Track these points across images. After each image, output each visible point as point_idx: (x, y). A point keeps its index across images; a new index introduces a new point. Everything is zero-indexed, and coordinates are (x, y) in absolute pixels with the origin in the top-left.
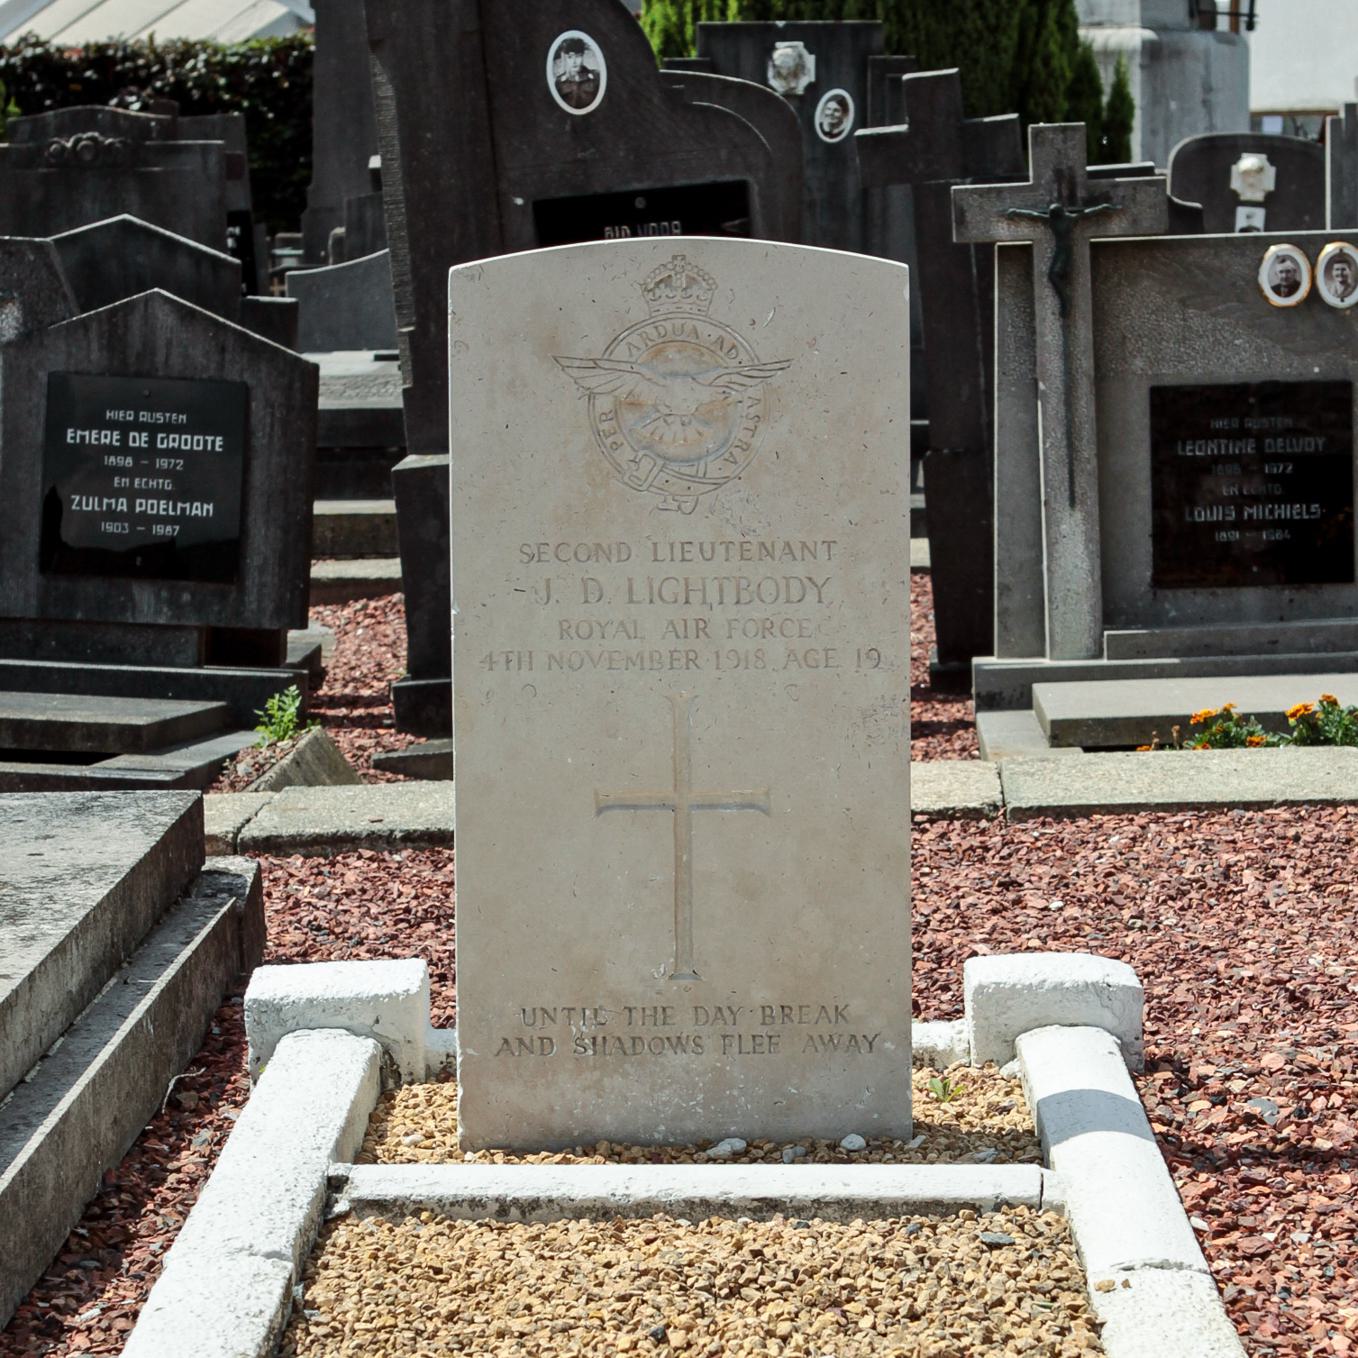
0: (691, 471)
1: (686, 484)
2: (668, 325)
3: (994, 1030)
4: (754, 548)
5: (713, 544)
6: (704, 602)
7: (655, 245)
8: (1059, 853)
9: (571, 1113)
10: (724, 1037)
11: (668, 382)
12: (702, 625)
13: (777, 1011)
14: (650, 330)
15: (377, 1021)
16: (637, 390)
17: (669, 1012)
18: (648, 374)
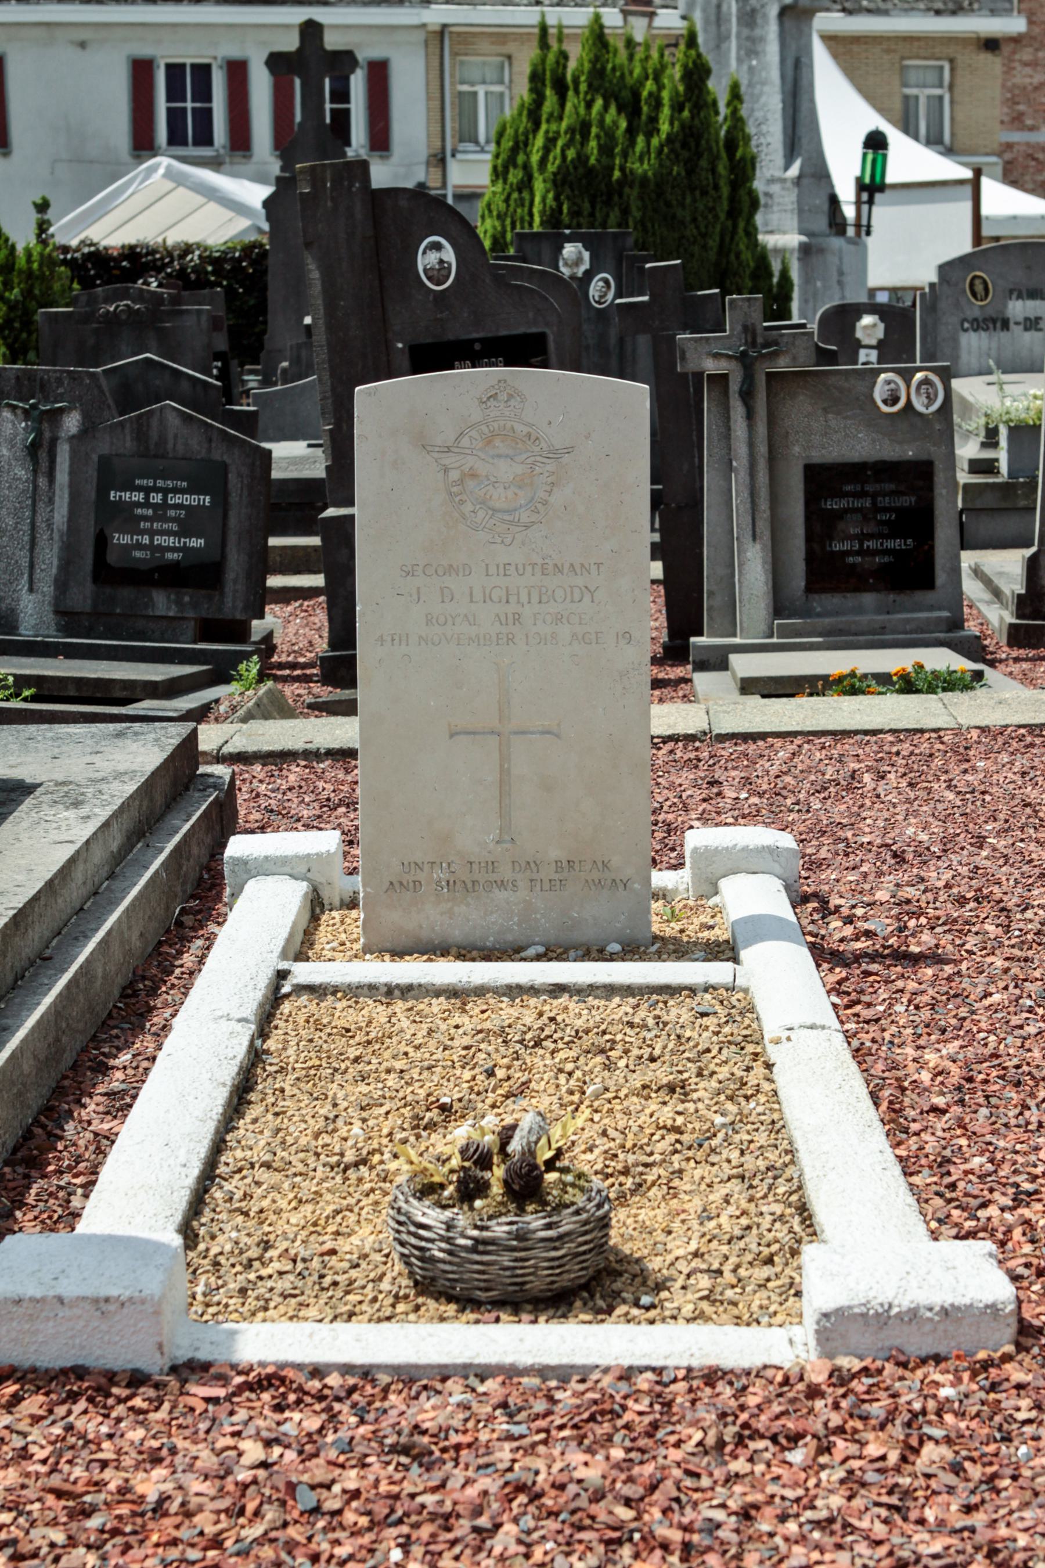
4: (550, 567)
7: (487, 373)
13: (565, 864)
14: (484, 428)
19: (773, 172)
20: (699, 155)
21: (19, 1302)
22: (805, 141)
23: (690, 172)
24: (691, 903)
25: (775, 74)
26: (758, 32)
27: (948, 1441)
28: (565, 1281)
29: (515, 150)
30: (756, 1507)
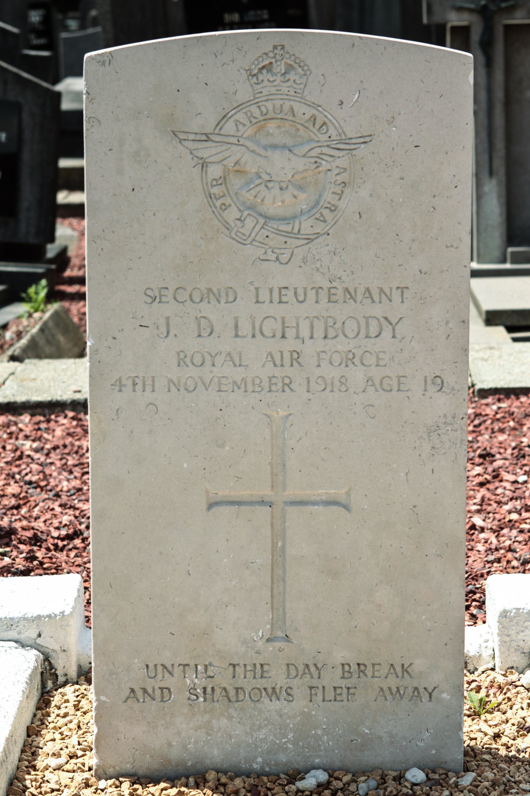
0: (289, 228)
1: (284, 239)
2: (269, 105)
3: (514, 644)
4: (340, 292)
5: (305, 289)
6: (297, 337)
7: (259, 37)
8: (512, 424)
9: (185, 747)
10: (311, 688)
11: (269, 153)
12: (295, 355)
13: (354, 667)
14: (254, 109)
15: (39, 635)
16: (243, 161)
17: (266, 668)
18: (252, 146)
24: (501, 680)
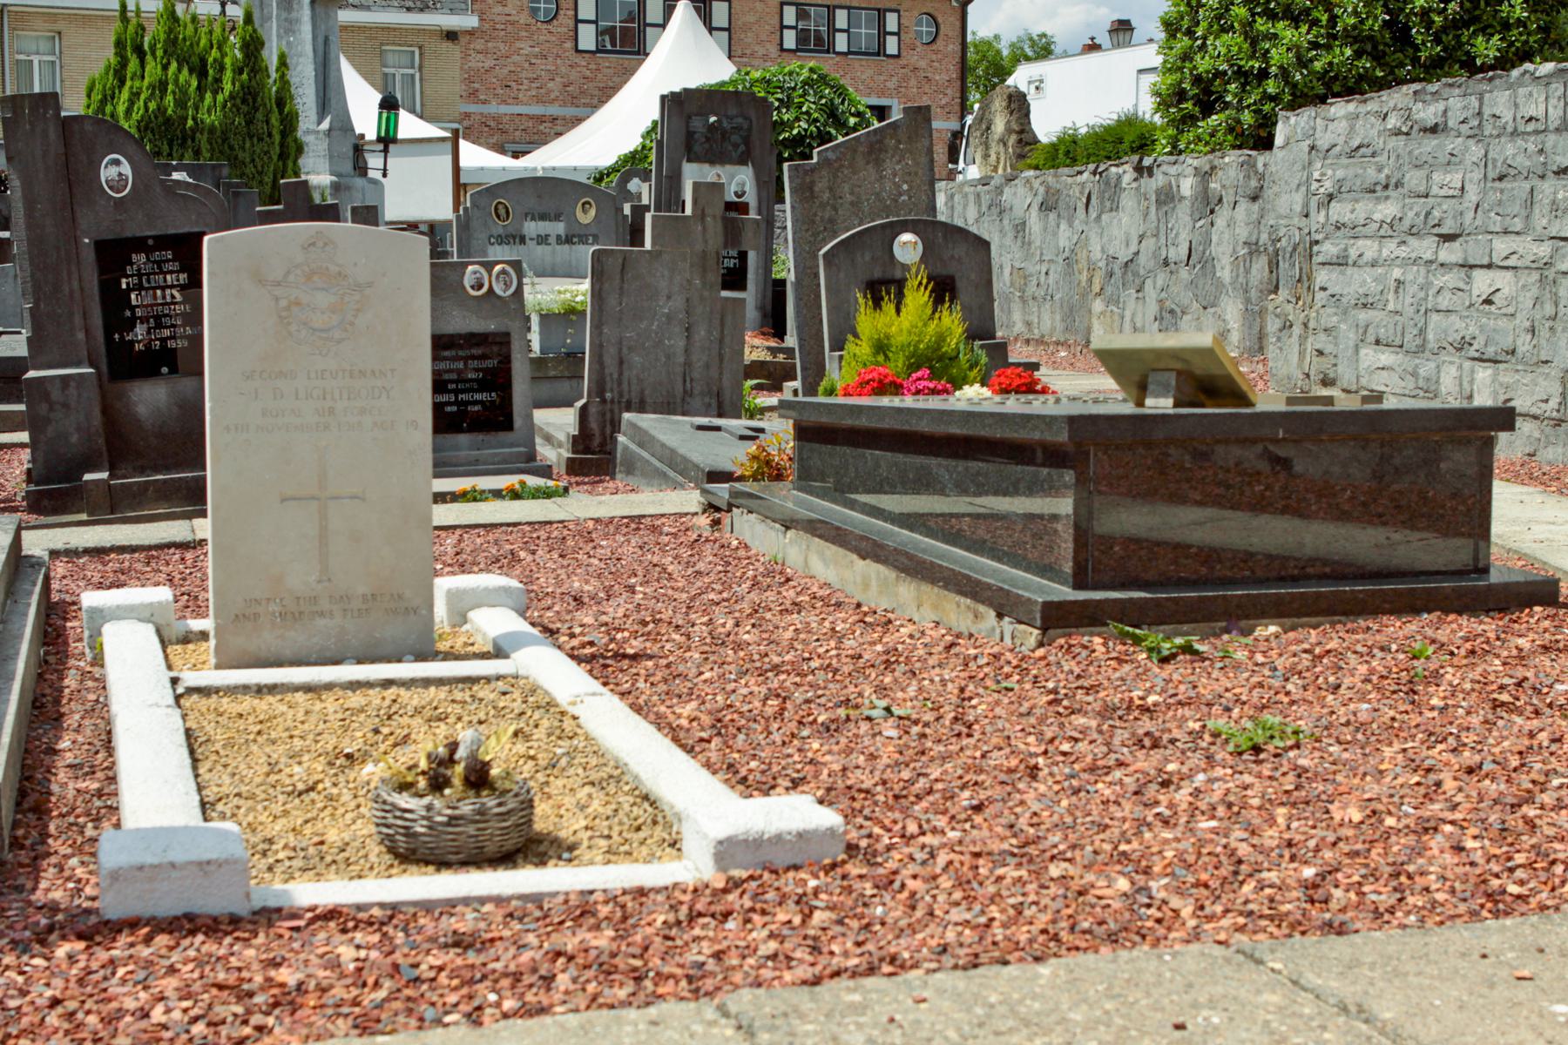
19: (310, 125)
20: (257, 110)
21: (141, 868)
22: (333, 102)
23: (249, 123)
25: (309, 48)
26: (294, 15)
27: (828, 908)
28: (509, 845)
29: (104, 102)
30: (723, 952)
